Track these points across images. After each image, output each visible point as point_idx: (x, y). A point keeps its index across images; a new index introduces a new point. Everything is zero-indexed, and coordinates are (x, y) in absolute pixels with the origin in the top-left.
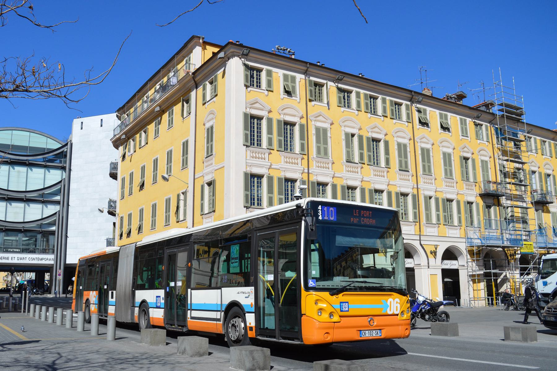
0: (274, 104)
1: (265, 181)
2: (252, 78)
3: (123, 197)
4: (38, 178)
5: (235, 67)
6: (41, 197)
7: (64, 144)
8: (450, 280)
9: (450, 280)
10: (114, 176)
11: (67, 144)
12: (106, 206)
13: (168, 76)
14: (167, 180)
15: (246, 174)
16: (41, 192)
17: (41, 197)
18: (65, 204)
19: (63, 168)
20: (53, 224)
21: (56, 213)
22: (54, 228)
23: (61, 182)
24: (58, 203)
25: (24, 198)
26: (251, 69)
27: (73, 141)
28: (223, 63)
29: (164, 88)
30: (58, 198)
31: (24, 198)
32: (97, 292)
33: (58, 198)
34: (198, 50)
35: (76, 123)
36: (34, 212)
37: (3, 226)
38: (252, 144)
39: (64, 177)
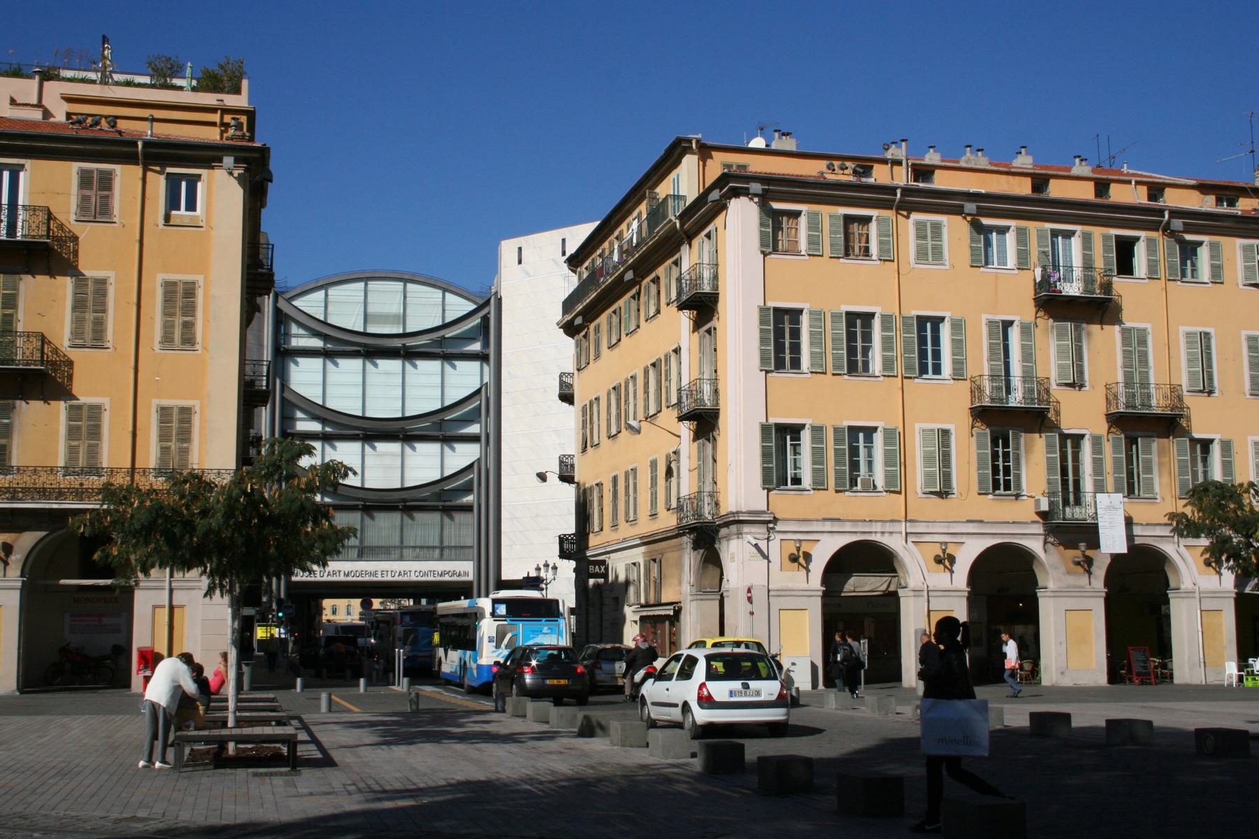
0: (825, 285)
1: (806, 436)
2: (773, 238)
3: (584, 449)
4: (427, 387)
5: (742, 216)
6: (438, 427)
7: (481, 302)
8: (63, 582)
9: (63, 582)
10: (567, 398)
11: (487, 303)
12: (556, 468)
13: (654, 197)
14: (639, 432)
15: (765, 429)
16: (436, 418)
17: (438, 427)
18: (493, 441)
19: (482, 357)
20: (467, 489)
21: (471, 466)
22: (470, 499)
23: (478, 392)
24: (474, 439)
25: (402, 431)
26: (776, 216)
27: (504, 294)
28: (721, 207)
29: (656, 214)
30: (474, 429)
31: (402, 431)
32: (915, 731)
33: (474, 429)
34: (689, 163)
35: (508, 248)
36: (425, 464)
37: (358, 499)
38: (780, 365)
39: (486, 379)
